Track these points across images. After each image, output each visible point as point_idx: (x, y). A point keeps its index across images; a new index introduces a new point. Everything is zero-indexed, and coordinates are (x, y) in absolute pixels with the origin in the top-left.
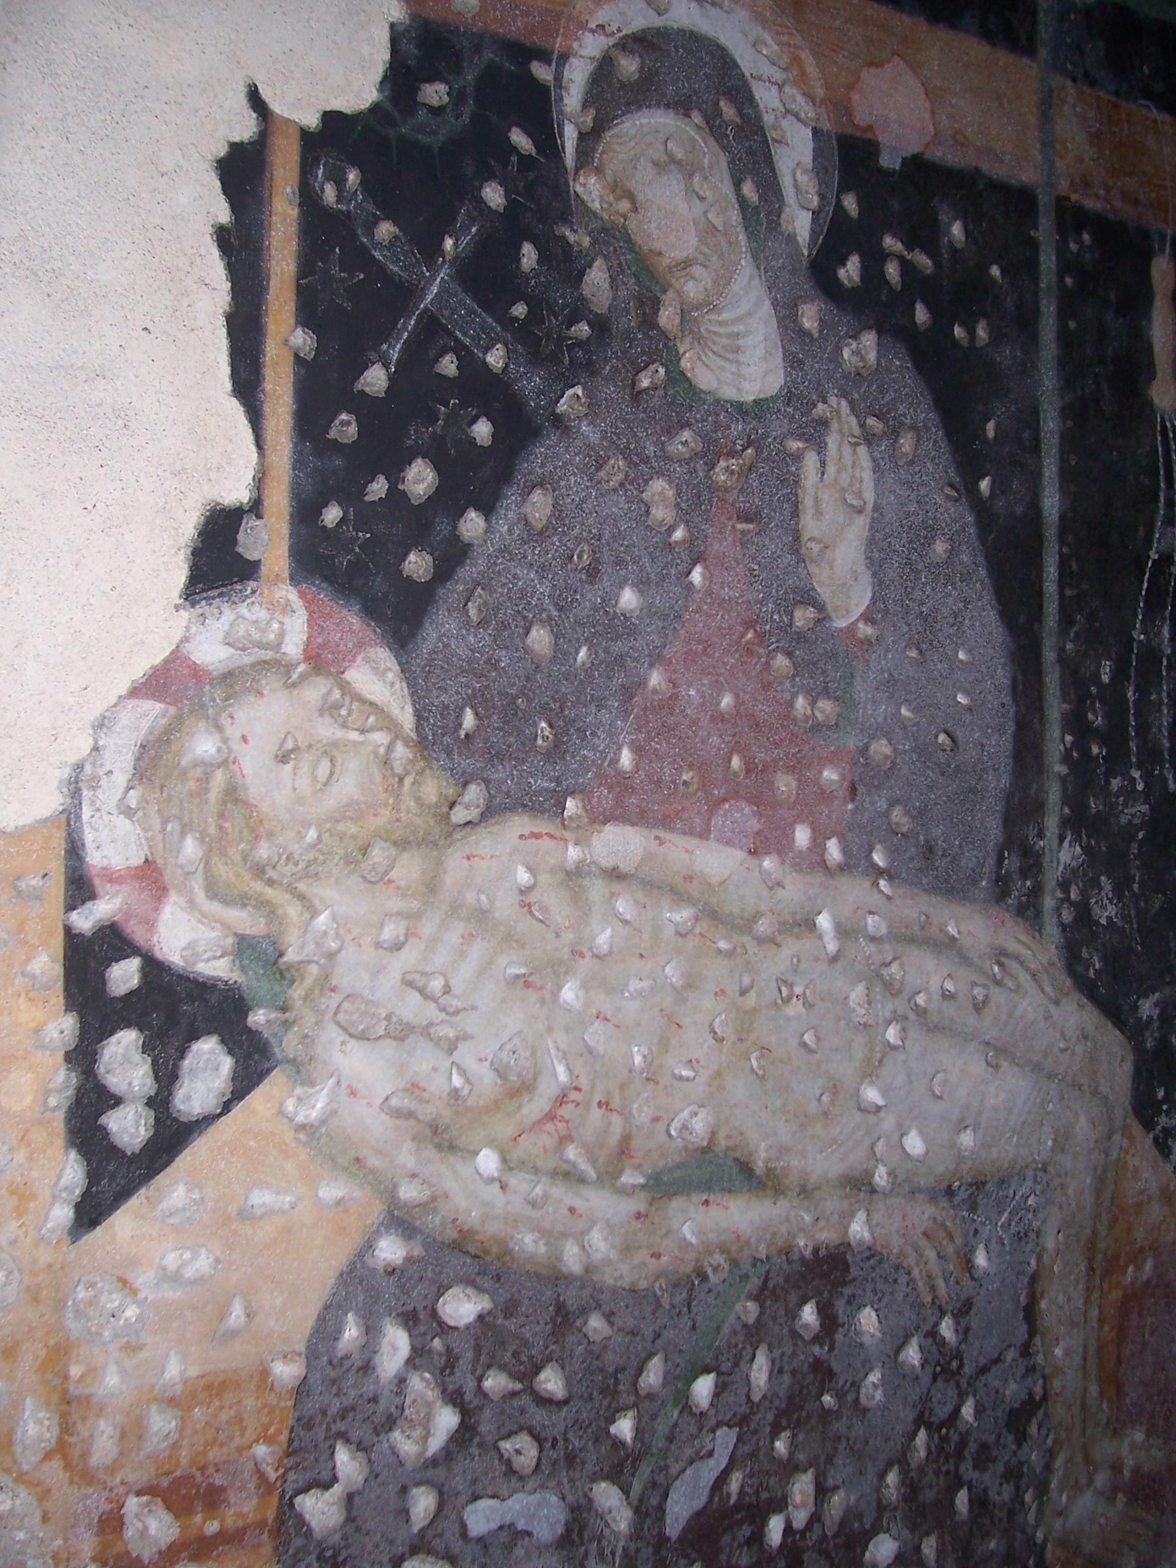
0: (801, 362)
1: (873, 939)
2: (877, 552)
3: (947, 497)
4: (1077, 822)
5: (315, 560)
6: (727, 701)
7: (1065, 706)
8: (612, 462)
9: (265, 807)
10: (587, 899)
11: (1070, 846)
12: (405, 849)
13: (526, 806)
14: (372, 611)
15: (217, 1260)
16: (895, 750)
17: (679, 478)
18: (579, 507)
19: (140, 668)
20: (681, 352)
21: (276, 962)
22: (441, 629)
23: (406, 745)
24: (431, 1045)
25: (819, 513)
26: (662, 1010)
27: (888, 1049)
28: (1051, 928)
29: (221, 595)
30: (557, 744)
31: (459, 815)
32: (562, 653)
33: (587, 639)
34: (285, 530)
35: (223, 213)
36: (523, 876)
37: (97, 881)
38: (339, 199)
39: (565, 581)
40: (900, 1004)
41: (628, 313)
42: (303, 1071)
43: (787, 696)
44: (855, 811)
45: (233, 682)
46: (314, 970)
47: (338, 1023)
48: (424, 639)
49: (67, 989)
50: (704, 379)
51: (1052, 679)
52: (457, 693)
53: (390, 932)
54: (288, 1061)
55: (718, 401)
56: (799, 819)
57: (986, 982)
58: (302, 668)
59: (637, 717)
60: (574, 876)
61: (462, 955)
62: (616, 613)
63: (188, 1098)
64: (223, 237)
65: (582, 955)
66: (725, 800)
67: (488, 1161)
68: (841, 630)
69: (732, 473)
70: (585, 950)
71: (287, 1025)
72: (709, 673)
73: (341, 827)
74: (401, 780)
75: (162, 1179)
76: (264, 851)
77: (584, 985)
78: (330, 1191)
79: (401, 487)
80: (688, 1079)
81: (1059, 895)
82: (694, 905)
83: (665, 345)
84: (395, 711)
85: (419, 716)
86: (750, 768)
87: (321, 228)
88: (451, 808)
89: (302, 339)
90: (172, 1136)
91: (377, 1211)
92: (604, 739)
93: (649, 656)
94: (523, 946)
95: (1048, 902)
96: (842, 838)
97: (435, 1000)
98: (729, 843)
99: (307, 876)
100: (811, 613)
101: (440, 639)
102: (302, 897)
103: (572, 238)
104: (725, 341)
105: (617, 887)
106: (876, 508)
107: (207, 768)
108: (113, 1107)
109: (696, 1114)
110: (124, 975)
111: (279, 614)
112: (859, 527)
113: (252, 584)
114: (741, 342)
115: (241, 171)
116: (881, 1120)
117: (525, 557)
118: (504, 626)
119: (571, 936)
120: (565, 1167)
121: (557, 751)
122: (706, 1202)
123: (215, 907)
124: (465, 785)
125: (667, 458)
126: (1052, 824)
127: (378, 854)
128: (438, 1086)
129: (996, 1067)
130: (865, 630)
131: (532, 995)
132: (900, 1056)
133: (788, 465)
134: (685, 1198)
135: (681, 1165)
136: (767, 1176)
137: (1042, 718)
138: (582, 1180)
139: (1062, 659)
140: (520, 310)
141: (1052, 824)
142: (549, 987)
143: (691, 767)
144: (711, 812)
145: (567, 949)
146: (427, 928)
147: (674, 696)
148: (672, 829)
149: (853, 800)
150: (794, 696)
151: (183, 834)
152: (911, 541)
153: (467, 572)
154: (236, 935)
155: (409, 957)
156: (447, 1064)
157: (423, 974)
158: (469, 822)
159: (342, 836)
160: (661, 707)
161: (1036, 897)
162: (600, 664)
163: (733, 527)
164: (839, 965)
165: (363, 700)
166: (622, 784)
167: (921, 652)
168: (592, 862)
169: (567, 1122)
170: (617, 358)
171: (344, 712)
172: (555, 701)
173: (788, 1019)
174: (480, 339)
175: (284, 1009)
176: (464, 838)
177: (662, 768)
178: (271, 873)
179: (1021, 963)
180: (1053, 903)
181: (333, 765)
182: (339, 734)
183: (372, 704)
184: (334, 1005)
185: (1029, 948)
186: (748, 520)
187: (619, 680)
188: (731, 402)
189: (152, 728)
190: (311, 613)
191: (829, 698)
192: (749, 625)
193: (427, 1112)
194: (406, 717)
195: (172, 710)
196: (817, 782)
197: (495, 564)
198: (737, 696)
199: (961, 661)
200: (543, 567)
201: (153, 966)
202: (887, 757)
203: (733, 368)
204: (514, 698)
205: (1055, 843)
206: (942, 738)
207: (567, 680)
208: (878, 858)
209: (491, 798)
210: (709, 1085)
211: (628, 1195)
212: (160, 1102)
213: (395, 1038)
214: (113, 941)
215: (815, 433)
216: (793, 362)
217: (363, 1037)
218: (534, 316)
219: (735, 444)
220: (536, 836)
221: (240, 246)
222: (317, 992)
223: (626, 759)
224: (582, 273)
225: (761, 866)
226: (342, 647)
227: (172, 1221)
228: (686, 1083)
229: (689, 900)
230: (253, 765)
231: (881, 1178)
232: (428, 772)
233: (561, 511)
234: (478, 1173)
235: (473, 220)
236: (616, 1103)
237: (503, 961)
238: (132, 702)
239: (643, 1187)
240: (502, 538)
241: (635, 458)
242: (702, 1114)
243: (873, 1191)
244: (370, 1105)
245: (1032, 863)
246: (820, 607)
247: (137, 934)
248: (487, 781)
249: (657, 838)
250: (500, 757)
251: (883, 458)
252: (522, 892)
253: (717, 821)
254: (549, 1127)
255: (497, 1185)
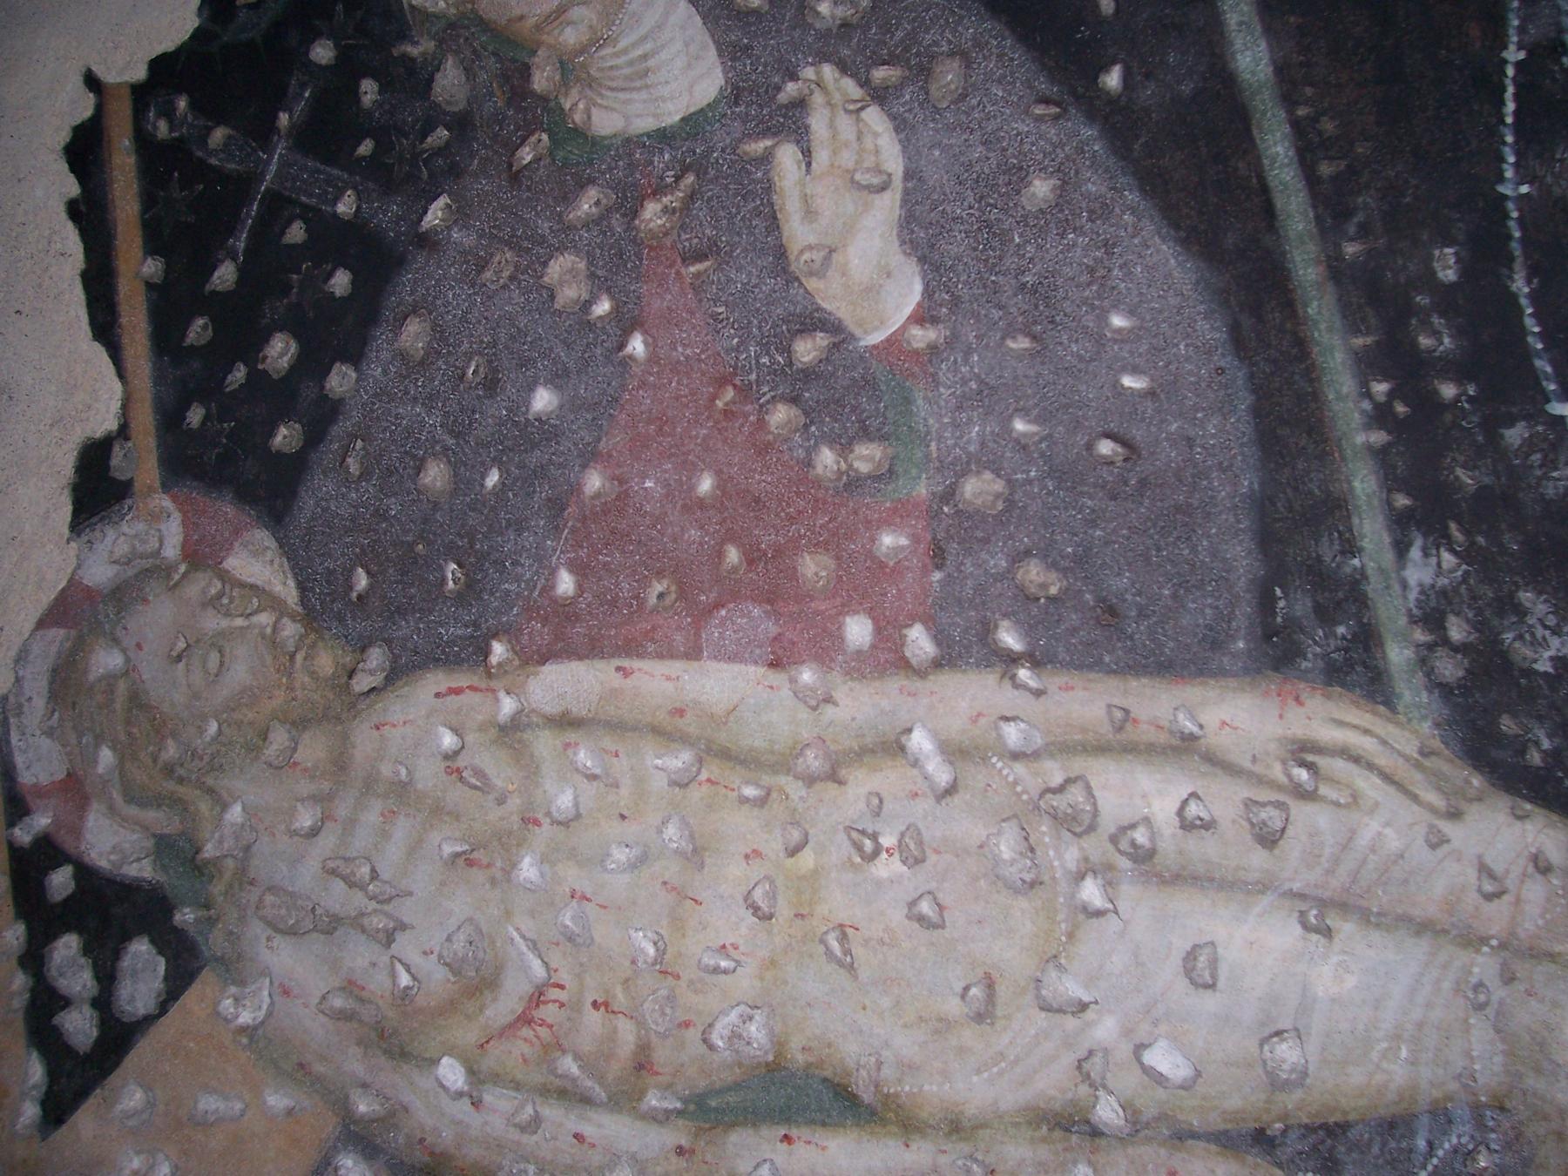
0: (748, 47)
1: (1016, 756)
2: (921, 233)
3: (1039, 119)
4: (1425, 515)
5: (185, 463)
6: (706, 485)
7: (1359, 341)
8: (497, 259)
9: (166, 708)
10: (532, 756)
11: (1426, 555)
12: (305, 728)
13: (438, 660)
14: (245, 495)
15: (176, 1167)
16: (1009, 481)
17: (589, 245)
18: (464, 319)
19: (47, 597)
20: (567, 106)
21: (194, 858)
22: (320, 494)
23: (293, 618)
24: (364, 937)
25: (810, 213)
26: (665, 883)
27: (1081, 917)
28: (1411, 691)
29: (101, 520)
30: (470, 585)
31: (362, 683)
32: (465, 480)
33: (494, 460)
34: (152, 442)
35: (73, 188)
36: (448, 740)
37: (29, 798)
38: (171, 130)
39: (459, 403)
40: (1097, 847)
41: (491, 94)
42: (235, 970)
43: (801, 453)
44: (948, 581)
45: (123, 595)
46: (230, 863)
47: (263, 919)
48: (301, 509)
49: (15, 898)
50: (606, 122)
51: (1321, 310)
52: (343, 554)
53: (305, 820)
54: (217, 960)
55: (628, 140)
56: (846, 609)
57: (1282, 797)
58: (183, 568)
59: (573, 531)
60: (510, 733)
61: (385, 835)
62: (527, 420)
63: (132, 999)
64: (74, 210)
65: (537, 823)
66: (718, 605)
67: (451, 1072)
68: (875, 347)
69: (674, 210)
70: (540, 816)
71: (211, 922)
72: (672, 455)
73: (237, 716)
74: (292, 656)
75: (114, 1079)
76: (171, 751)
77: (544, 859)
78: (277, 1101)
79: (260, 367)
80: (725, 972)
81: (1420, 636)
82: (692, 745)
83: (544, 109)
84: (278, 589)
85: (302, 588)
86: (752, 558)
87: (157, 161)
88: (350, 677)
89: (152, 267)
90: (118, 1037)
91: (330, 1126)
92: (531, 566)
93: (579, 456)
94: (457, 818)
95: (1397, 655)
96: (929, 621)
97: (362, 887)
98: (733, 658)
99: (212, 769)
100: (822, 339)
101: (317, 505)
102: (211, 791)
103: (414, 51)
104: (627, 71)
105: (572, 736)
106: (908, 175)
107: (111, 679)
108: (63, 1008)
109: (751, 1018)
110: (61, 881)
111: (159, 524)
112: (888, 206)
113: (129, 502)
114: (651, 63)
115: (84, 151)
116: (1089, 1025)
117: (407, 393)
118: (390, 472)
119: (518, 801)
120: (558, 1082)
121: (471, 589)
122: (787, 1138)
123: (133, 811)
124: (363, 650)
125: (570, 228)
126: (1372, 531)
127: (279, 738)
128: (378, 983)
129: (1328, 933)
130: (922, 337)
131: (478, 875)
132: (1112, 923)
133: (749, 173)
134: (751, 1131)
135: (736, 1086)
136: (885, 1104)
137: (1311, 373)
138: (586, 1100)
139: (1336, 271)
140: (366, 148)
141: (1372, 531)
142: (499, 864)
143: (660, 574)
144: (698, 625)
145: (515, 818)
146: (342, 810)
147: (623, 496)
148: (640, 656)
149: (939, 567)
150: (811, 452)
151: (97, 746)
152: (982, 198)
153: (338, 430)
154: (154, 835)
155: (327, 842)
156: (386, 959)
157: (346, 859)
158: (374, 689)
159: (239, 724)
160: (605, 512)
161: (1367, 649)
162: (514, 484)
163: (678, 273)
164: (956, 800)
165: (242, 585)
166: (565, 612)
167: (1034, 338)
168: (533, 711)
169: (550, 1027)
170: (486, 147)
171: (225, 601)
172: (462, 537)
173: (879, 883)
174: (326, 192)
175: (207, 907)
176: (369, 707)
177: (617, 584)
178: (181, 772)
179: (1356, 760)
180: (1409, 653)
181: (222, 656)
182: (225, 623)
183: (253, 587)
184: (254, 898)
185: (1366, 732)
186: (700, 256)
187: (543, 492)
188: (648, 135)
189: (59, 652)
190: (184, 514)
191: (871, 440)
192: (722, 382)
193: (367, 1013)
194: (288, 591)
195: (73, 633)
196: (870, 555)
197: (372, 411)
198: (718, 473)
199: (1119, 331)
200: (430, 397)
201: (85, 872)
202: (998, 496)
203: (644, 95)
204: (412, 545)
205: (1389, 557)
206: (1106, 447)
207: (474, 510)
208: (1010, 639)
209: (395, 659)
210: (762, 979)
211: (660, 1122)
212: (103, 1002)
213: (323, 932)
214: (48, 852)
215: (791, 122)
216: (730, 53)
217: (292, 932)
218: (382, 147)
219: (662, 178)
220: (457, 691)
221: (89, 214)
222: (236, 886)
223: (566, 583)
224: (431, 80)
225: (793, 681)
226: (218, 538)
227: (130, 1123)
228: (723, 977)
229: (685, 740)
230: (150, 669)
231: (1107, 1112)
232: (320, 644)
233: (442, 332)
234: (442, 1086)
235: (303, 86)
236: (620, 999)
237: (435, 837)
238: (41, 632)
239: (680, 1113)
240: (376, 381)
241: (525, 244)
242: (759, 1016)
243: (1095, 1133)
244: (306, 1006)
245: (1343, 598)
246: (833, 327)
247: (67, 842)
248: (388, 642)
249: (618, 669)
250: (401, 612)
251: (910, 110)
252: (447, 757)
253: (712, 631)
254: (526, 1032)
255: (466, 1100)
